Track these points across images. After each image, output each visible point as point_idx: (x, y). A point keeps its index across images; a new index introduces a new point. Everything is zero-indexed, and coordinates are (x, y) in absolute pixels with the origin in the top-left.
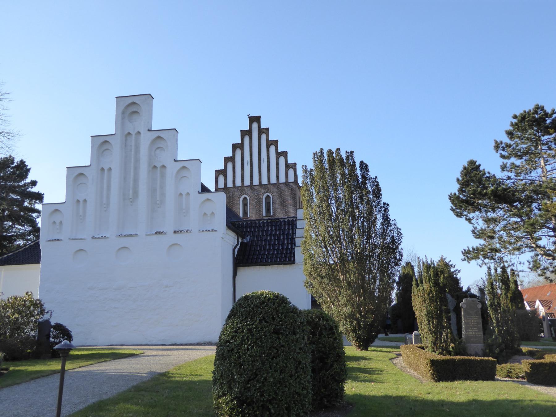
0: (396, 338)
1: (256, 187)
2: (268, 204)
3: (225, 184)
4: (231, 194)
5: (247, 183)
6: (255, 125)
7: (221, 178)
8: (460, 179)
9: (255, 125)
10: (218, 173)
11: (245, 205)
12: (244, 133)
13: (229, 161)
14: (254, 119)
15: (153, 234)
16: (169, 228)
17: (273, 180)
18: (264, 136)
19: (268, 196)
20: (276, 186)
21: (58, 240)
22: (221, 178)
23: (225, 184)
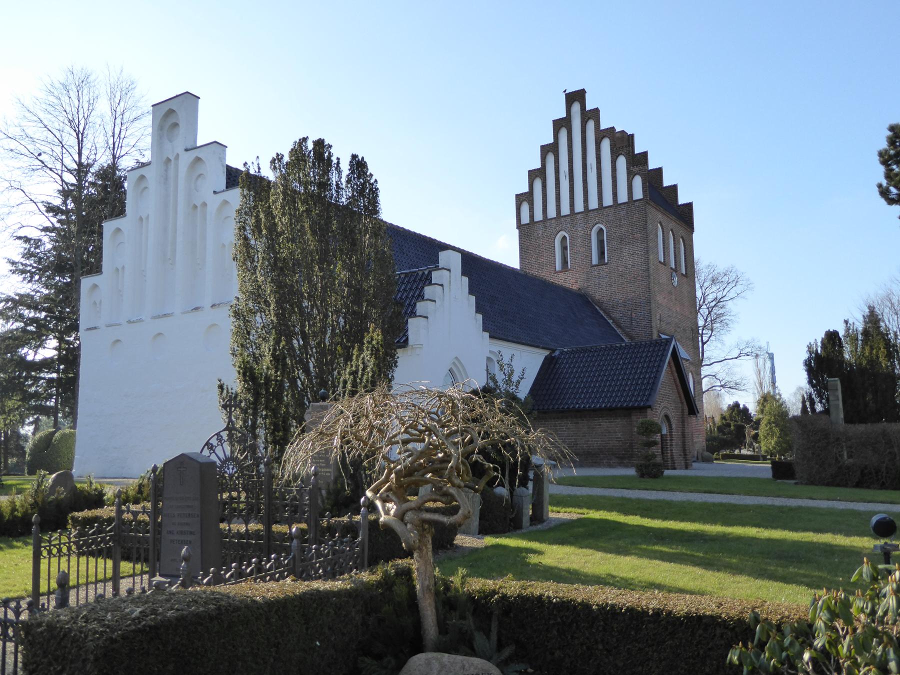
0: (614, 478)
1: (579, 216)
2: (601, 243)
3: (532, 216)
4: (541, 232)
5: (565, 210)
6: (576, 107)
7: (525, 207)
8: (286, 159)
9: (576, 107)
10: (521, 199)
11: (564, 248)
12: (559, 125)
13: (537, 176)
14: (576, 97)
15: (188, 312)
16: (207, 303)
17: (608, 201)
18: (591, 125)
19: (601, 229)
20: (612, 209)
21: (95, 328)
22: (525, 207)
23: (532, 216)
